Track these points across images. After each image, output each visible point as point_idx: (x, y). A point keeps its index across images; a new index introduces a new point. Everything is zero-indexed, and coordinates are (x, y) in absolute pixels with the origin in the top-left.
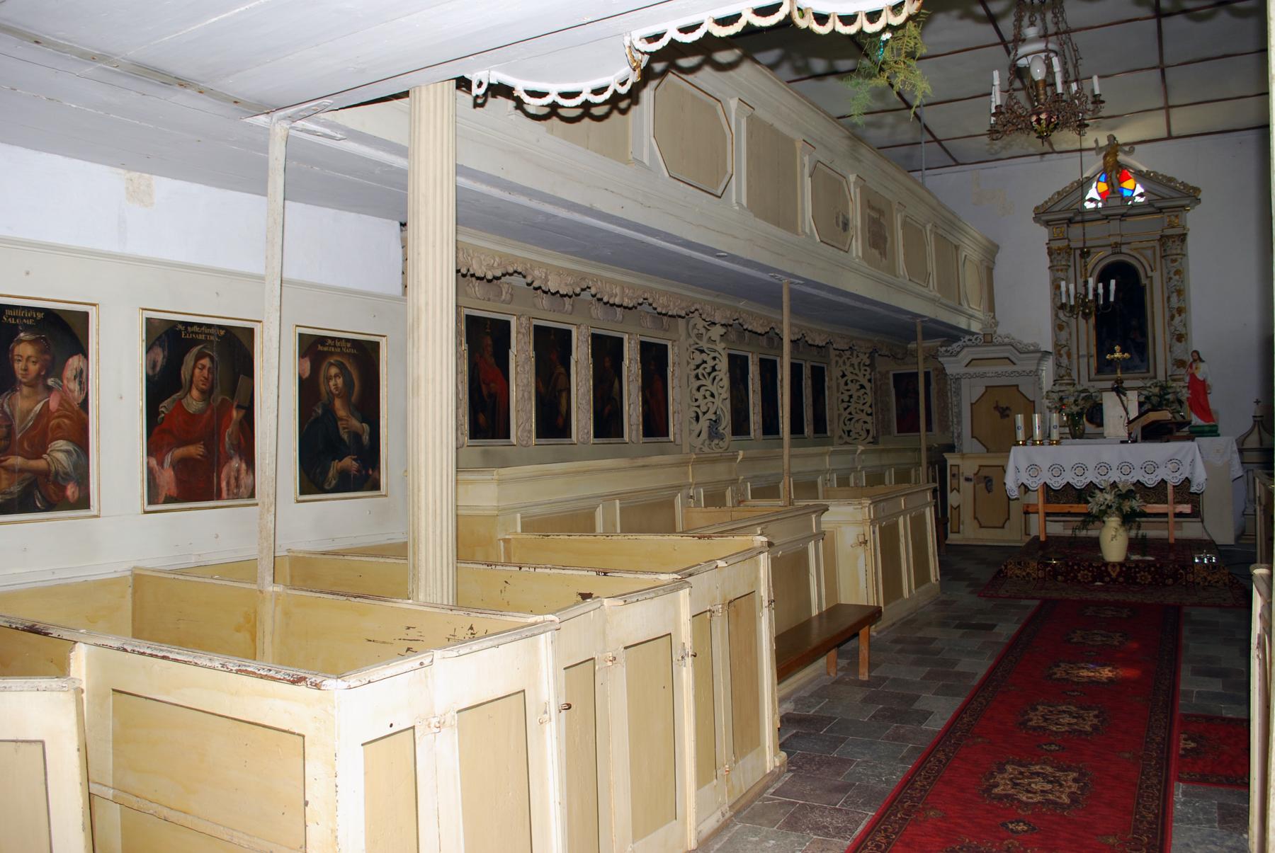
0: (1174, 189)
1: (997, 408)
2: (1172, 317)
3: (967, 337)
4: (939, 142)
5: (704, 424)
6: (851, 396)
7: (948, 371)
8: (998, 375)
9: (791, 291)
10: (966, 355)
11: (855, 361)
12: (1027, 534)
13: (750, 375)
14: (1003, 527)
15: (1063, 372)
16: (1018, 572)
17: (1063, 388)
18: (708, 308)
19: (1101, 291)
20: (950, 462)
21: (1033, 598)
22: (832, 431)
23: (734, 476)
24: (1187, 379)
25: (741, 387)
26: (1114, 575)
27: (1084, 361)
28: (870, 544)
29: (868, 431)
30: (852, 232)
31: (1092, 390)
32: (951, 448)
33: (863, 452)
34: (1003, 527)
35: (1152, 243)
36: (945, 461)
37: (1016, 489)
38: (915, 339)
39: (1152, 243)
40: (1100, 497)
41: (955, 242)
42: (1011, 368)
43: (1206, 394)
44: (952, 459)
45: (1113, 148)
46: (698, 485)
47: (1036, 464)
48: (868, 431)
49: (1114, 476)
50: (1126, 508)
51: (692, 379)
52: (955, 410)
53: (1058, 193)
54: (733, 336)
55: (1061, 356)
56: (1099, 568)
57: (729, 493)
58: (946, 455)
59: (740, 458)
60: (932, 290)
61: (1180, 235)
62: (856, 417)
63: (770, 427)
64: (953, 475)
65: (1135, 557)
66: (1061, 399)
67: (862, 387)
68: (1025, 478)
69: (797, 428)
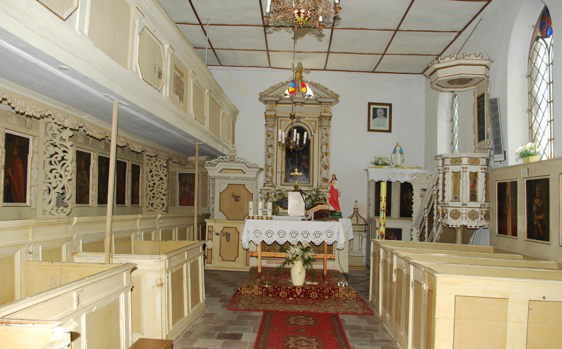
0: (327, 93)
1: (233, 196)
2: (323, 157)
3: (221, 157)
4: (213, 49)
5: (54, 195)
6: (154, 184)
7: (210, 174)
8: (236, 179)
9: (119, 111)
10: (220, 166)
11: (158, 164)
12: (247, 265)
13: (92, 166)
14: (235, 261)
15: (269, 180)
16: (247, 291)
17: (269, 188)
18: (59, 115)
19: (298, 137)
20: (208, 224)
21: (258, 310)
22: (142, 203)
23: (69, 235)
24: (329, 188)
25: (85, 172)
26: (299, 294)
27: (279, 175)
28: (165, 286)
29: (163, 204)
30: (164, 80)
31: (283, 190)
32: (208, 216)
33: (160, 218)
34: (235, 261)
35: (315, 119)
36: (206, 223)
37: (247, 243)
38: (194, 155)
39: (315, 119)
40: (292, 250)
41: (220, 105)
42: (242, 175)
43: (337, 196)
44: (209, 223)
45: (300, 70)
46: (36, 243)
47: (257, 230)
48: (163, 204)
49: (300, 238)
50: (306, 257)
51: (47, 164)
52: (211, 195)
53: (272, 87)
54: (81, 139)
55: (268, 171)
56: (291, 290)
57: (64, 248)
58: (206, 220)
59: (74, 222)
60: (206, 126)
61: (329, 117)
62: (157, 196)
63: (102, 200)
64: (210, 232)
65: (309, 283)
66: (268, 194)
67: (161, 179)
68: (252, 237)
69: (120, 199)
